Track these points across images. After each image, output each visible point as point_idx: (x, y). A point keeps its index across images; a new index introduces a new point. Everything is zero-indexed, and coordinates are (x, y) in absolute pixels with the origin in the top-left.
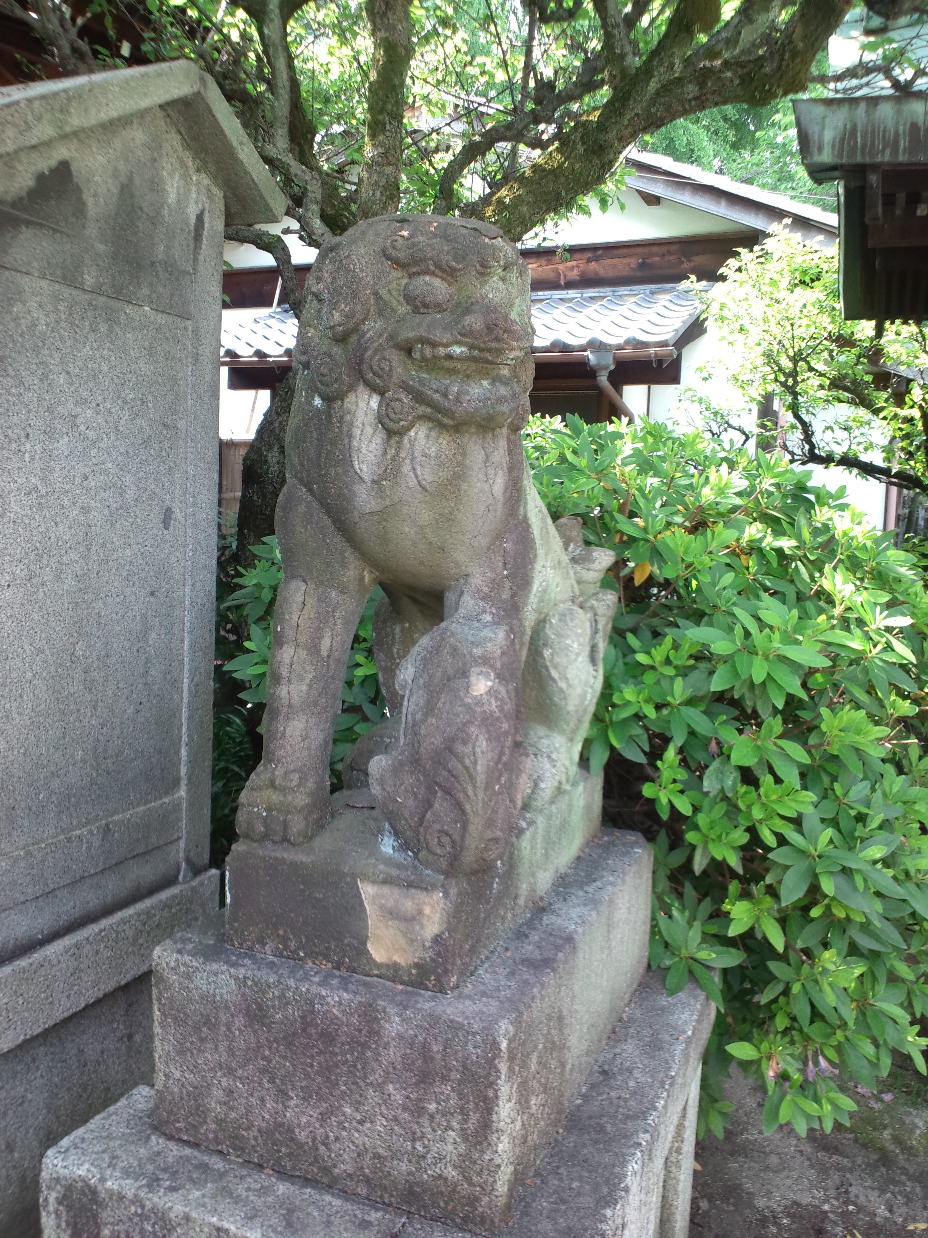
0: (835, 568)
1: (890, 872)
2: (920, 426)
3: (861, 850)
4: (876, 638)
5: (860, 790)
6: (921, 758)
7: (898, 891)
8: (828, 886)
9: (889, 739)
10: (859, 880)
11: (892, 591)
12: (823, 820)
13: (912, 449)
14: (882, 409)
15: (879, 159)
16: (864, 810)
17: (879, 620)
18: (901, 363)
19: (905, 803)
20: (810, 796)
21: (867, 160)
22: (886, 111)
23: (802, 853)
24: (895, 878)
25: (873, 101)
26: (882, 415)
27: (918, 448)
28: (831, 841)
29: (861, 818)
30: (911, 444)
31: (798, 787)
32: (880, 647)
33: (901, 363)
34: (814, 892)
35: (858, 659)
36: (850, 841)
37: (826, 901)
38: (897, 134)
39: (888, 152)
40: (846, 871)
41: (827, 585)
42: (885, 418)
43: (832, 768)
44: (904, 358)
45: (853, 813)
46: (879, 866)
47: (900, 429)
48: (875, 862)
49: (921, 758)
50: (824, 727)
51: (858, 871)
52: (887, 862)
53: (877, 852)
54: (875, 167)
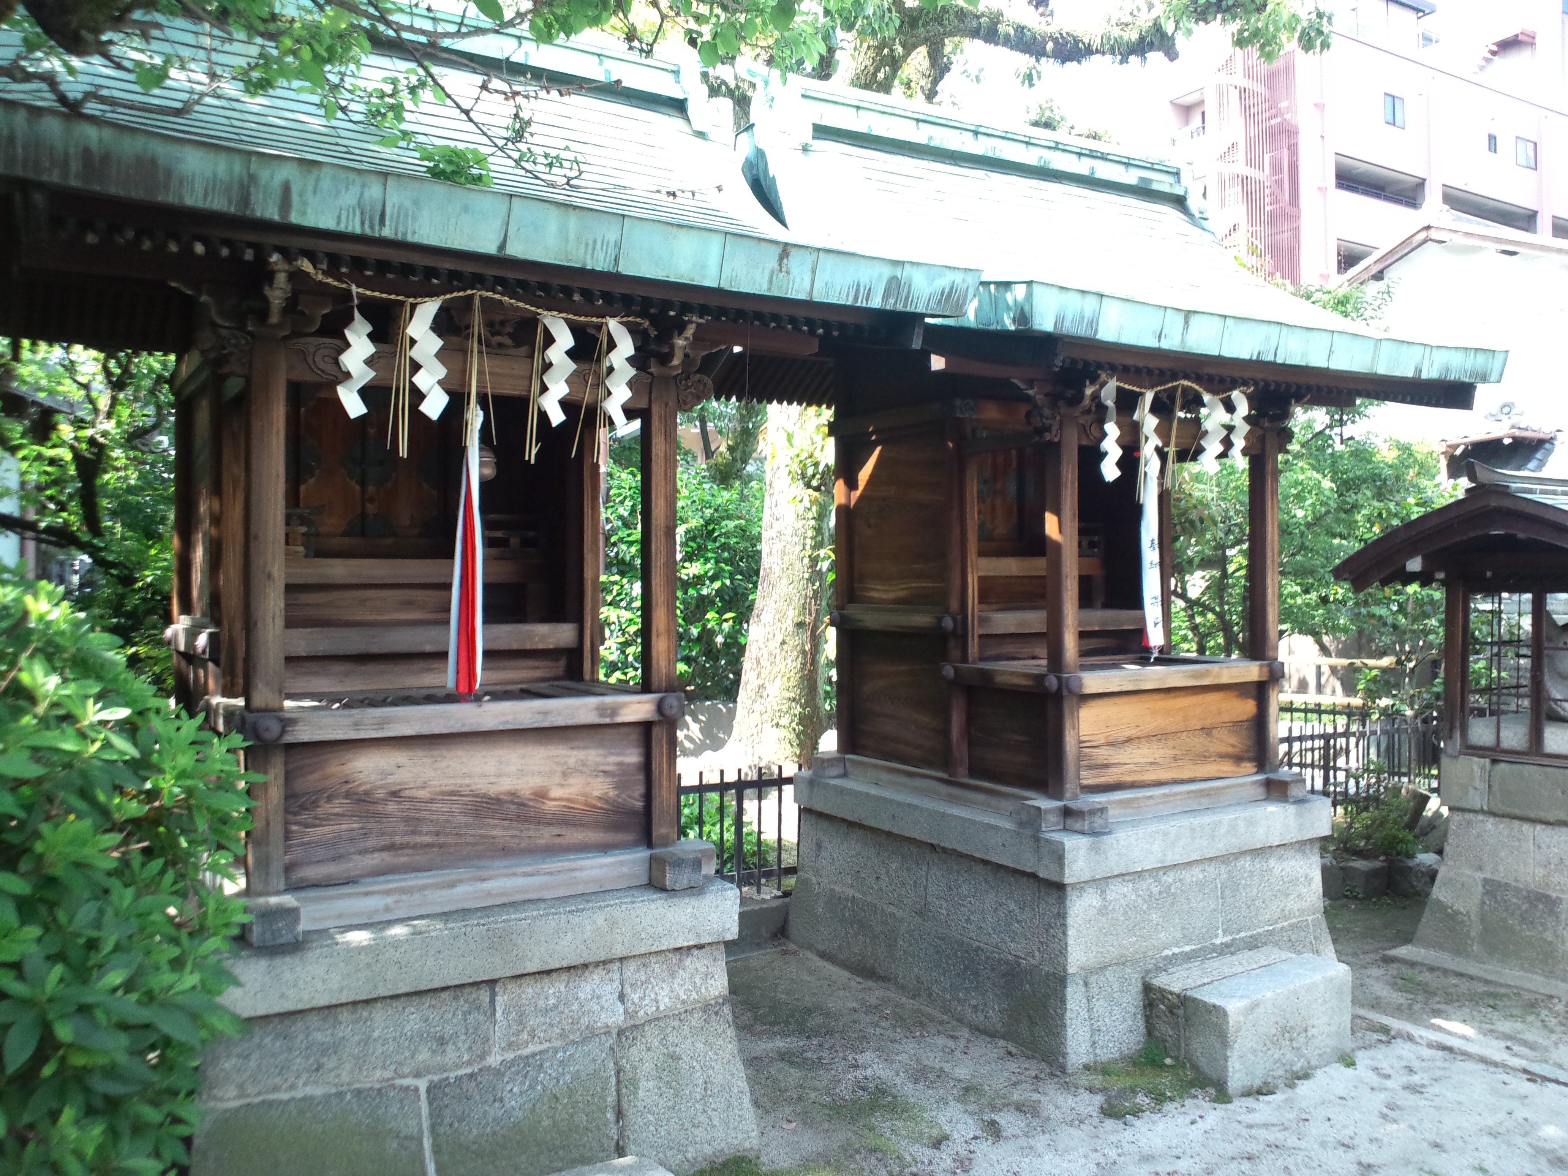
0: (32, 657)
1: (133, 997)
2: (72, 471)
3: (99, 979)
4: (93, 735)
5: (86, 913)
6: (143, 865)
7: (144, 1015)
8: (64, 1032)
9: (116, 848)
10: (100, 1015)
11: (99, 678)
12: (48, 958)
13: (64, 498)
14: (20, 447)
15: (45, 178)
16: (94, 934)
17: (92, 713)
18: (41, 389)
19: (139, 916)
20: (33, 931)
21: (31, 175)
22: (52, 127)
23: (27, 1003)
24: (139, 1002)
25: (36, 112)
26: (21, 454)
27: (71, 497)
28: (61, 980)
29: (92, 945)
30: (61, 492)
31: (16, 924)
32: (98, 745)
33: (41, 389)
34: (47, 1045)
35: (70, 761)
36: (82, 973)
37: (61, 1052)
38: (67, 154)
39: (56, 172)
40: (84, 1010)
41: (25, 678)
42: (24, 459)
43: (50, 894)
44: (44, 382)
45: (81, 941)
46: (120, 993)
47: (46, 473)
48: (115, 990)
49: (143, 865)
50: (39, 847)
51: (97, 1005)
52: (128, 986)
53: (115, 978)
54: (41, 186)
